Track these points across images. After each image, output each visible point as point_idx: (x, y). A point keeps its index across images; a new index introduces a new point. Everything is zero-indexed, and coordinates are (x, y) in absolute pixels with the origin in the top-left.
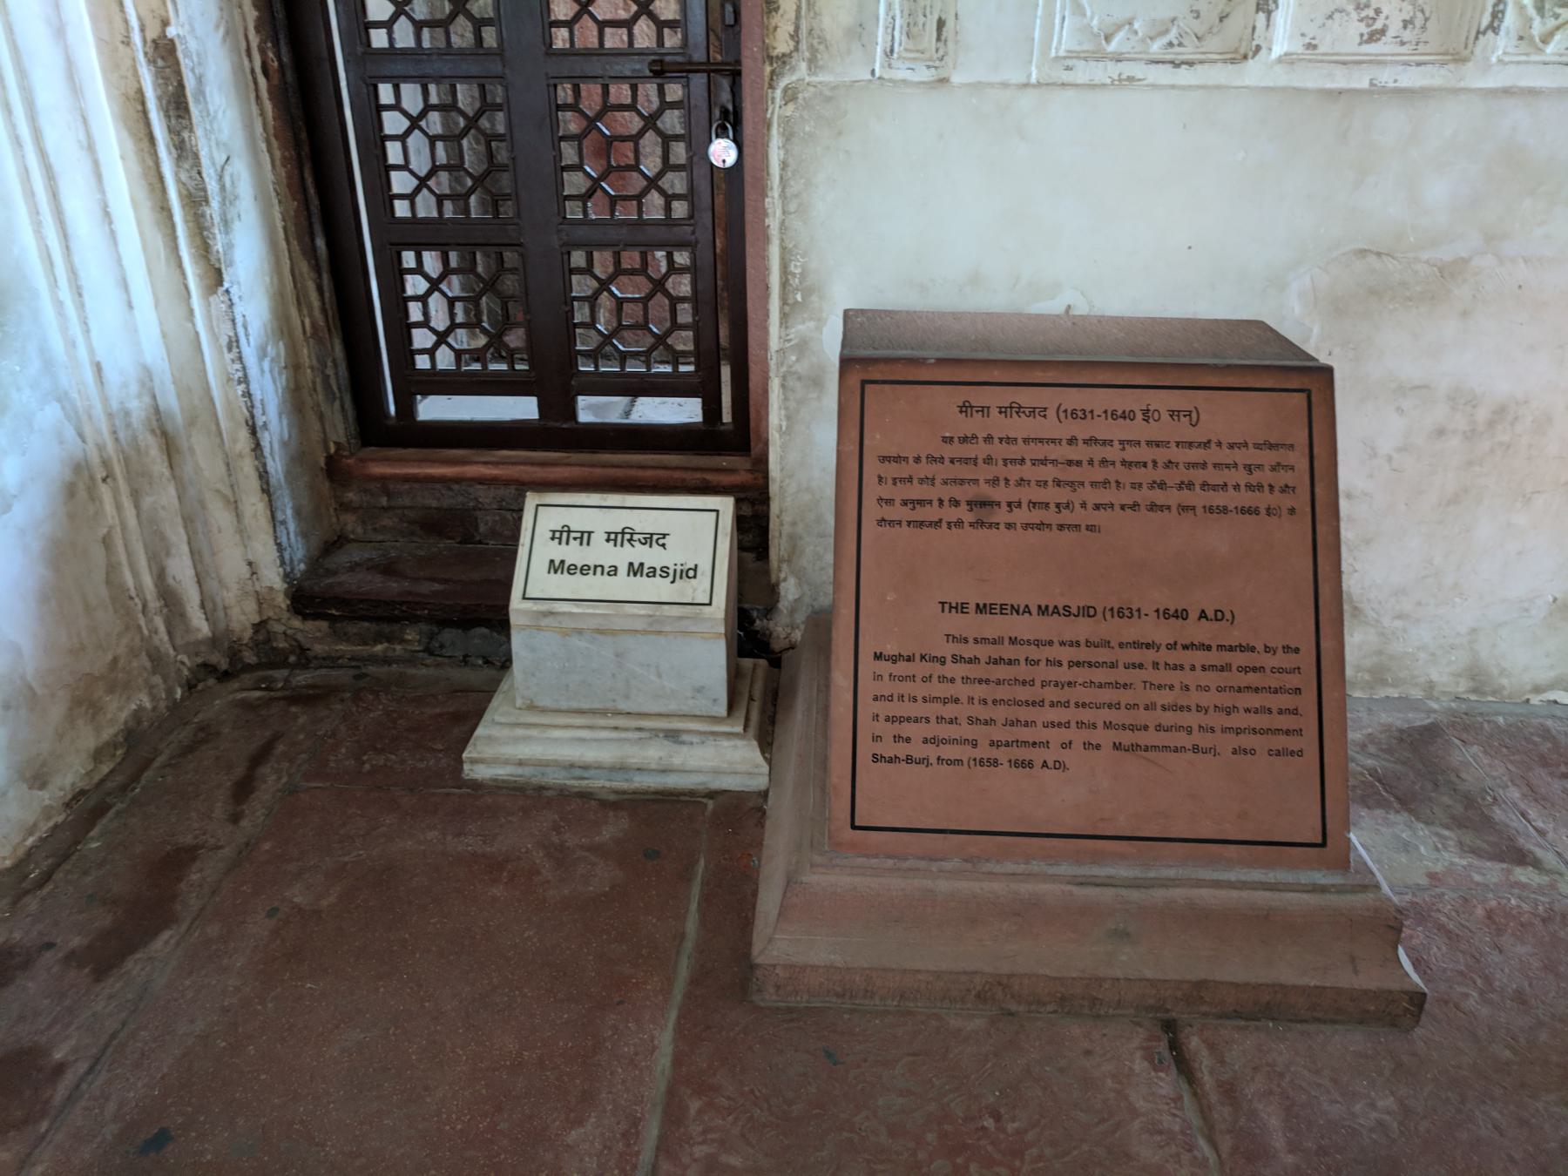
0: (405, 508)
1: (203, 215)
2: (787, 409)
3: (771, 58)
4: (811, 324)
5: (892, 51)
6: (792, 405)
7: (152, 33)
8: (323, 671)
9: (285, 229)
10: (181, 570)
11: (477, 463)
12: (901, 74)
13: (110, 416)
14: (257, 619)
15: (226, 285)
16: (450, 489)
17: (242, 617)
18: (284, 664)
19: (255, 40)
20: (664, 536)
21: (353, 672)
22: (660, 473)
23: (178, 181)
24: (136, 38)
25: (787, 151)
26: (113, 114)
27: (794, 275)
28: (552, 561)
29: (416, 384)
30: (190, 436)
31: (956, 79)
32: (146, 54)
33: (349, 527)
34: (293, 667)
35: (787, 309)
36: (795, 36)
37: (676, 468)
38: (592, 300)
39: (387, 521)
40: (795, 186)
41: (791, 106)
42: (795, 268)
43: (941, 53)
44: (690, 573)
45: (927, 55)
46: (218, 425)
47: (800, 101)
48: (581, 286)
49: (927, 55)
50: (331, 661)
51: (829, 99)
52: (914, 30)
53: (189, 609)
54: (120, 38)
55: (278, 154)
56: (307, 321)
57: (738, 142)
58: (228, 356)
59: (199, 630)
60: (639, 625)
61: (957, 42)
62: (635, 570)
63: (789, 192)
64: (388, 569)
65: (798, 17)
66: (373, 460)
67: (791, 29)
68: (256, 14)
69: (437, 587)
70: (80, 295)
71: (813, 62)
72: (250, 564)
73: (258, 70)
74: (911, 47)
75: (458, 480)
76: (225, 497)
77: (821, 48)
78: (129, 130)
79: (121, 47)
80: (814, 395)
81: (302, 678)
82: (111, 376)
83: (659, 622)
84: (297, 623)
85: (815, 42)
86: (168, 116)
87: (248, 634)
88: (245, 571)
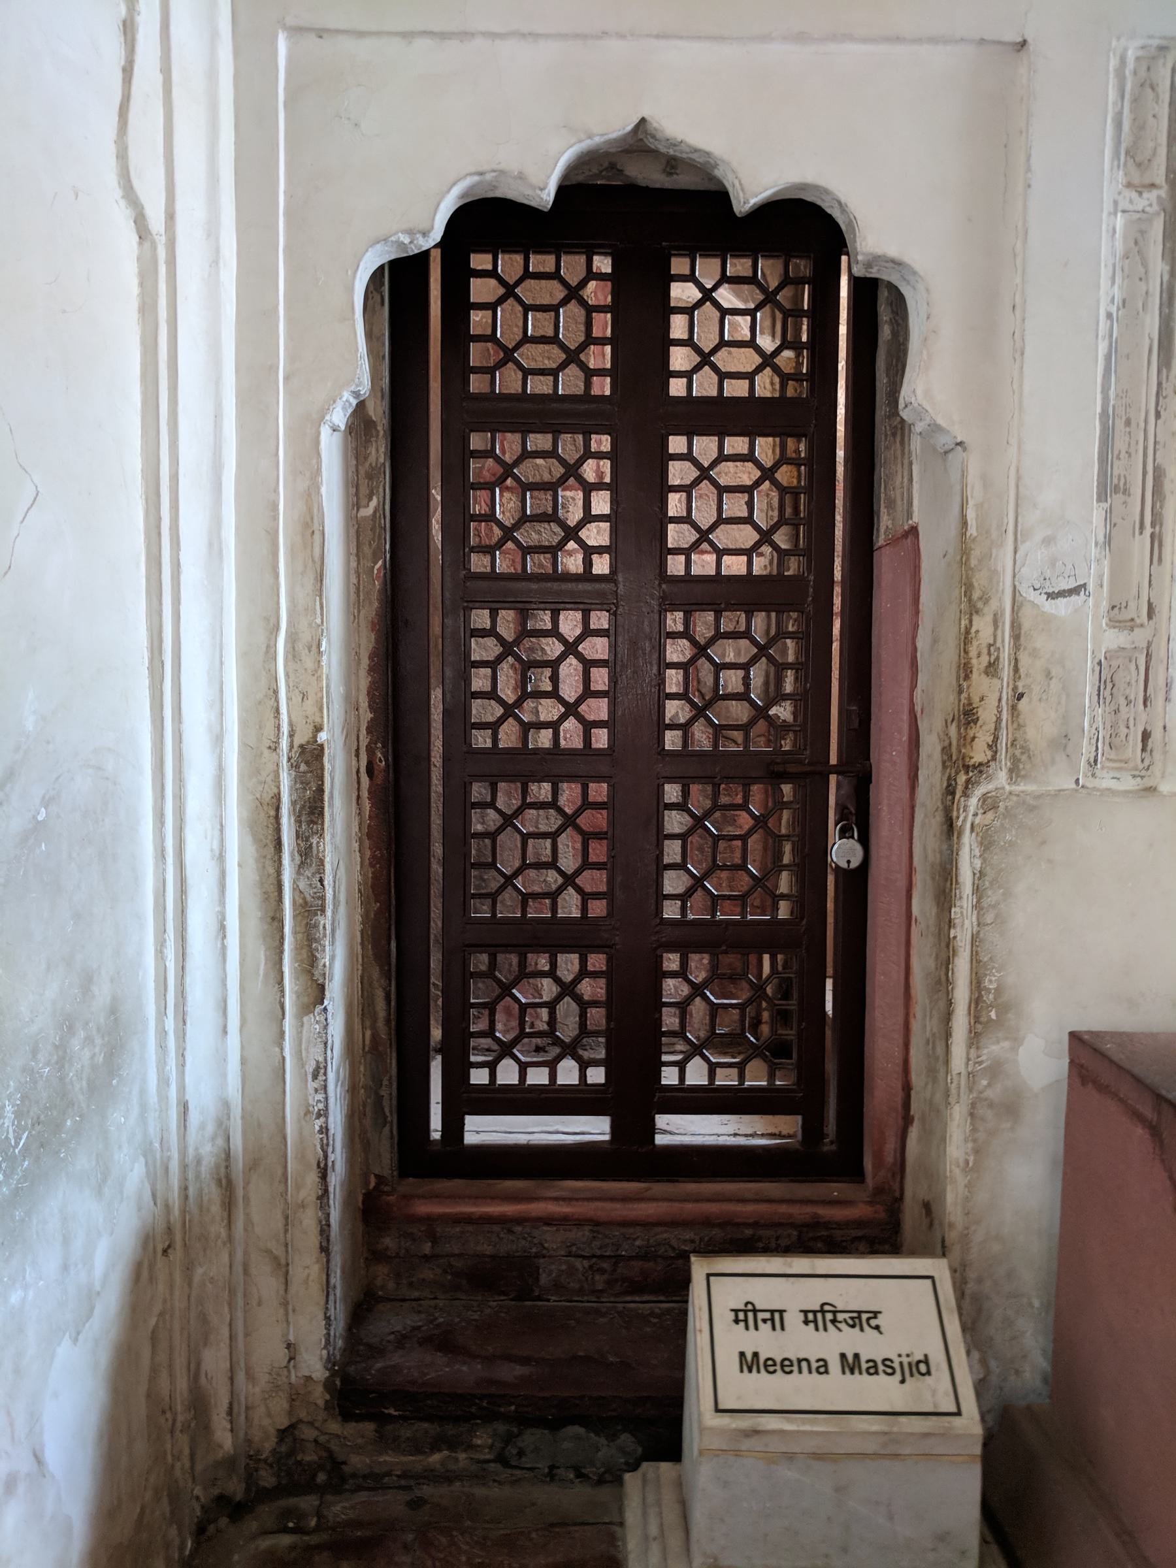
0: (453, 1255)
1: (316, 926)
2: (975, 1141)
3: (967, 768)
4: (1006, 1044)
5: (1096, 761)
6: (981, 1136)
7: (299, 740)
8: (363, 1496)
9: (362, 932)
10: (215, 1361)
11: (546, 1199)
12: (1106, 781)
13: (184, 1167)
14: (284, 1423)
15: (326, 1002)
16: (510, 1231)
17: (270, 1417)
18: (308, 1487)
19: (364, 740)
20: (876, 1314)
21: (405, 1497)
22: (763, 1208)
23: (296, 888)
24: (284, 743)
25: (984, 861)
26: (240, 820)
27: (988, 991)
28: (742, 1354)
29: (465, 1100)
30: (247, 1183)
31: (1164, 788)
32: (289, 759)
33: (379, 1282)
34: (321, 1490)
35: (979, 1027)
36: (993, 746)
37: (782, 1201)
38: (683, 1007)
39: (427, 1273)
40: (991, 897)
41: (990, 815)
42: (990, 983)
43: (1147, 763)
44: (920, 1368)
45: (1131, 765)
46: (286, 1167)
47: (1001, 809)
48: (673, 989)
49: (1131, 765)
50: (374, 1481)
51: (1032, 809)
52: (1116, 741)
53: (215, 1418)
54: (268, 743)
55: (368, 853)
56: (368, 1033)
57: (864, 841)
58: (312, 1085)
59: (220, 1446)
60: (871, 1447)
61: (1165, 753)
62: (851, 1364)
63: (986, 902)
64: (443, 1342)
65: (997, 728)
66: (419, 1197)
67: (990, 739)
68: (370, 716)
69: (520, 1370)
70: (184, 1023)
71: (1014, 772)
72: (289, 1346)
73: (363, 770)
74: (1113, 756)
75: (520, 1220)
76: (276, 1258)
77: (1024, 758)
78: (254, 835)
79: (266, 752)
80: (1009, 1125)
81: (340, 1509)
82: (194, 1118)
83: (894, 1444)
84: (334, 1427)
85: (1018, 752)
86: (299, 821)
87: (269, 1445)
88: (282, 1355)
